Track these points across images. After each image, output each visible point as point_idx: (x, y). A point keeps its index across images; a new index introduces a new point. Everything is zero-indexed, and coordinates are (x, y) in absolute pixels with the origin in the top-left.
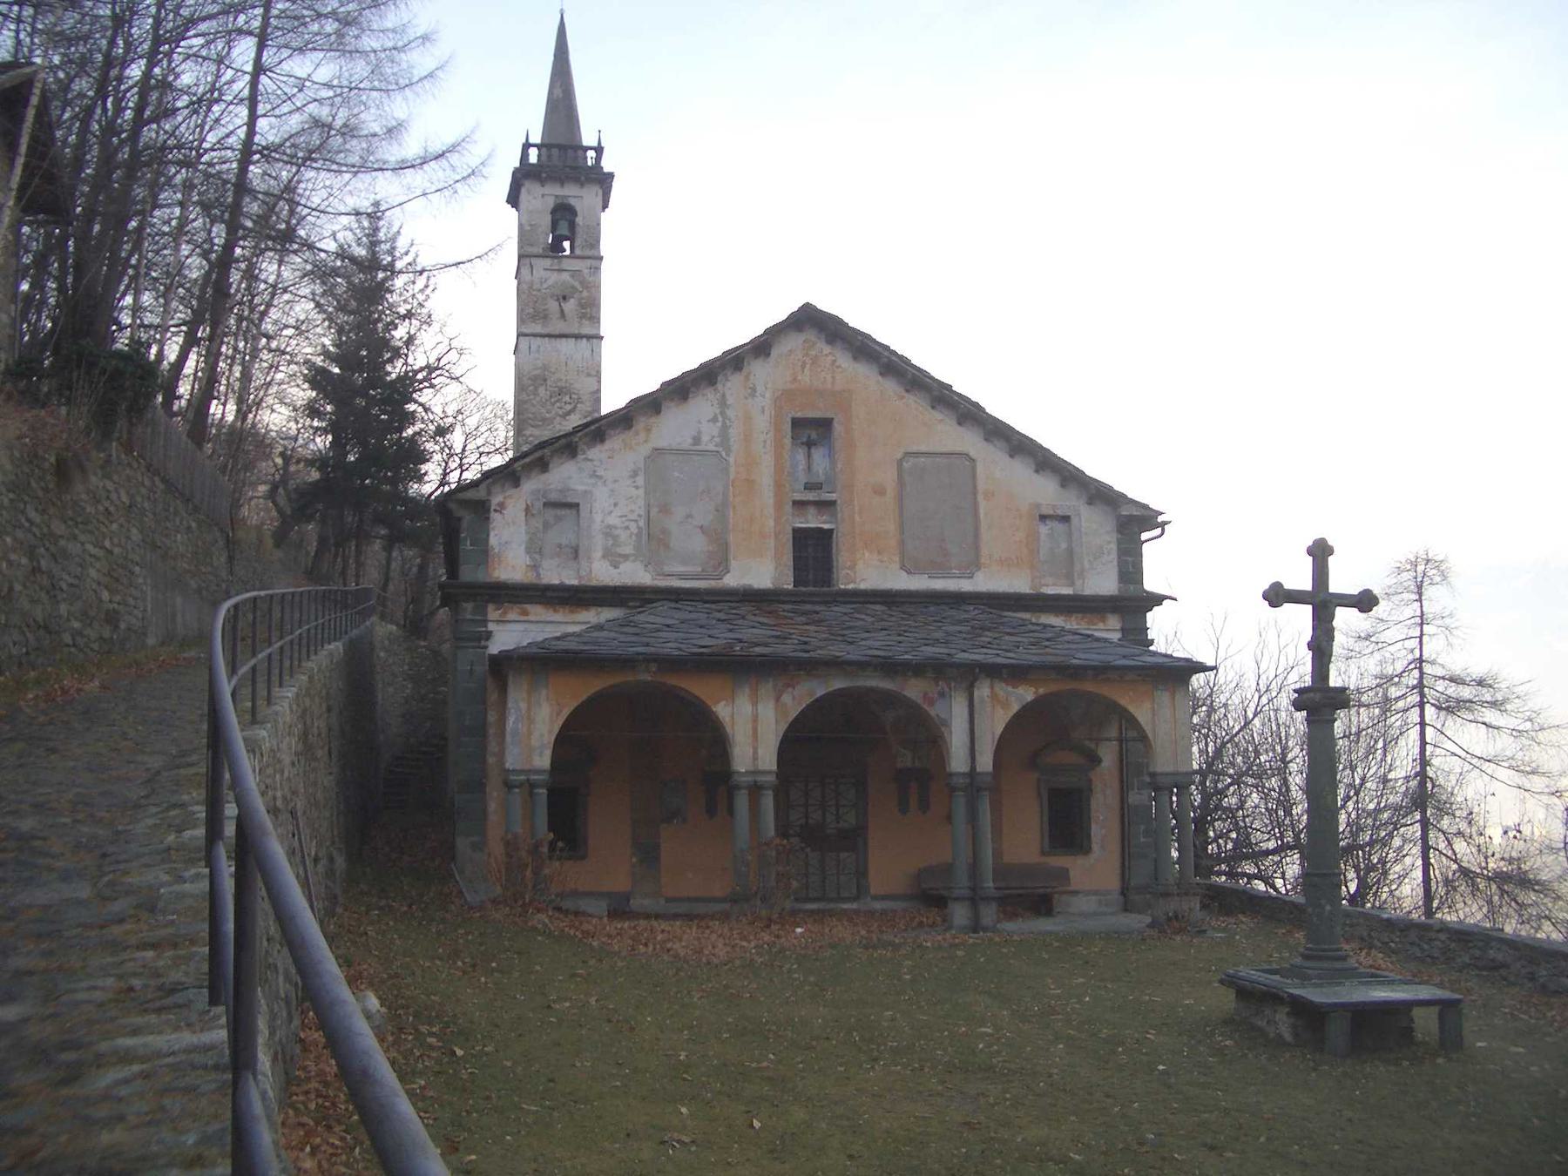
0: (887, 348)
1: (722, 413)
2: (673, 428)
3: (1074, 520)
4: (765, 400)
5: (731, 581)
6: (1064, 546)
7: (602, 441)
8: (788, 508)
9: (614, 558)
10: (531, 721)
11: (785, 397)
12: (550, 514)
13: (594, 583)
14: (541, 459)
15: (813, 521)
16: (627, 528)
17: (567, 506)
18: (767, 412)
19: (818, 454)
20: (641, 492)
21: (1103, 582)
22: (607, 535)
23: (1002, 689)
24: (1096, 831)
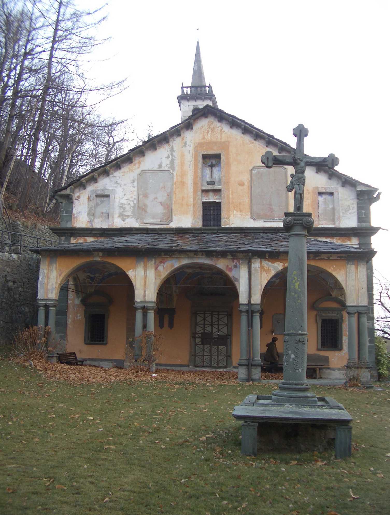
0: (243, 121)
1: (172, 154)
2: (151, 160)
3: (335, 194)
4: (191, 148)
5: (173, 225)
6: (331, 206)
7: (120, 169)
8: (200, 193)
9: (123, 216)
10: (48, 278)
11: (200, 145)
12: (99, 200)
13: (115, 227)
14: (93, 176)
15: (212, 198)
16: (129, 204)
17: (104, 196)
18: (191, 153)
19: (215, 170)
20: (136, 189)
21: (350, 221)
22: (121, 207)
23: (266, 264)
24: (345, 340)
